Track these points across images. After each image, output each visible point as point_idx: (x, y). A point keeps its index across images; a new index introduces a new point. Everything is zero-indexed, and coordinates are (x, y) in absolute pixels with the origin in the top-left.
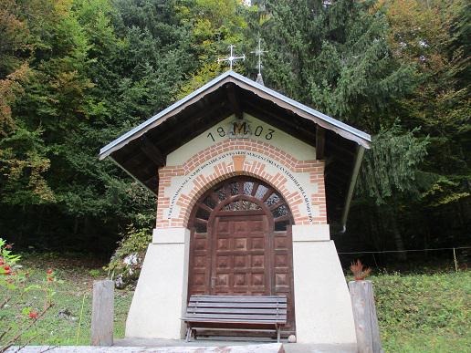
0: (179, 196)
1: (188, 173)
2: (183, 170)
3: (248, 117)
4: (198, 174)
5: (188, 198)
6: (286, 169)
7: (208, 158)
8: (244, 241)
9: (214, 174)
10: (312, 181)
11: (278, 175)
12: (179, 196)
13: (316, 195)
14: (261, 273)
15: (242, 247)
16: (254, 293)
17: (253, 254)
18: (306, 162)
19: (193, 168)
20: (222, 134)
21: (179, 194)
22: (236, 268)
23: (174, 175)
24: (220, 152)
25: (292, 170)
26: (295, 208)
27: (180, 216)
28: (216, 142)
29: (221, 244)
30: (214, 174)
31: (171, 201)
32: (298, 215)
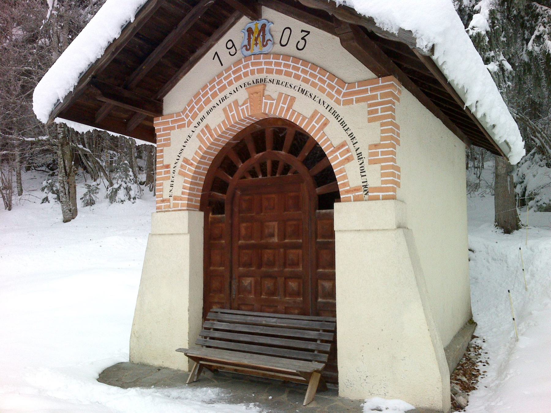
0: (180, 162)
1: (189, 123)
2: (183, 120)
3: (268, 13)
4: (203, 125)
5: (191, 164)
6: (328, 101)
7: (214, 95)
8: (274, 226)
9: (185, 182)
10: (370, 120)
11: (316, 113)
12: (180, 162)
13: (376, 146)
14: (295, 277)
15: (272, 235)
16: (287, 311)
17: (287, 247)
18: (360, 82)
19: (195, 116)
20: (233, 51)
21: (181, 159)
22: (288, 270)
23: (173, 128)
24: (230, 83)
25: (338, 102)
26: (341, 171)
27: (183, 193)
28: (225, 65)
29: (243, 232)
30: (185, 182)
31: (172, 171)
32: (344, 185)
